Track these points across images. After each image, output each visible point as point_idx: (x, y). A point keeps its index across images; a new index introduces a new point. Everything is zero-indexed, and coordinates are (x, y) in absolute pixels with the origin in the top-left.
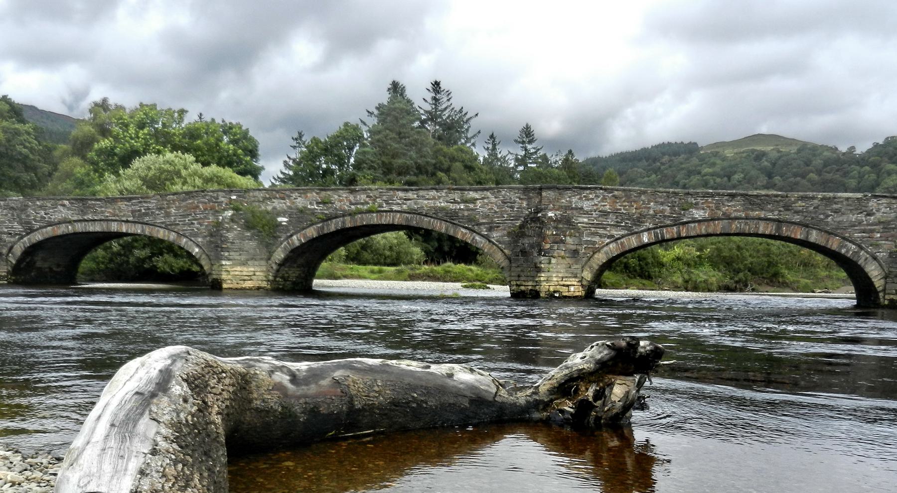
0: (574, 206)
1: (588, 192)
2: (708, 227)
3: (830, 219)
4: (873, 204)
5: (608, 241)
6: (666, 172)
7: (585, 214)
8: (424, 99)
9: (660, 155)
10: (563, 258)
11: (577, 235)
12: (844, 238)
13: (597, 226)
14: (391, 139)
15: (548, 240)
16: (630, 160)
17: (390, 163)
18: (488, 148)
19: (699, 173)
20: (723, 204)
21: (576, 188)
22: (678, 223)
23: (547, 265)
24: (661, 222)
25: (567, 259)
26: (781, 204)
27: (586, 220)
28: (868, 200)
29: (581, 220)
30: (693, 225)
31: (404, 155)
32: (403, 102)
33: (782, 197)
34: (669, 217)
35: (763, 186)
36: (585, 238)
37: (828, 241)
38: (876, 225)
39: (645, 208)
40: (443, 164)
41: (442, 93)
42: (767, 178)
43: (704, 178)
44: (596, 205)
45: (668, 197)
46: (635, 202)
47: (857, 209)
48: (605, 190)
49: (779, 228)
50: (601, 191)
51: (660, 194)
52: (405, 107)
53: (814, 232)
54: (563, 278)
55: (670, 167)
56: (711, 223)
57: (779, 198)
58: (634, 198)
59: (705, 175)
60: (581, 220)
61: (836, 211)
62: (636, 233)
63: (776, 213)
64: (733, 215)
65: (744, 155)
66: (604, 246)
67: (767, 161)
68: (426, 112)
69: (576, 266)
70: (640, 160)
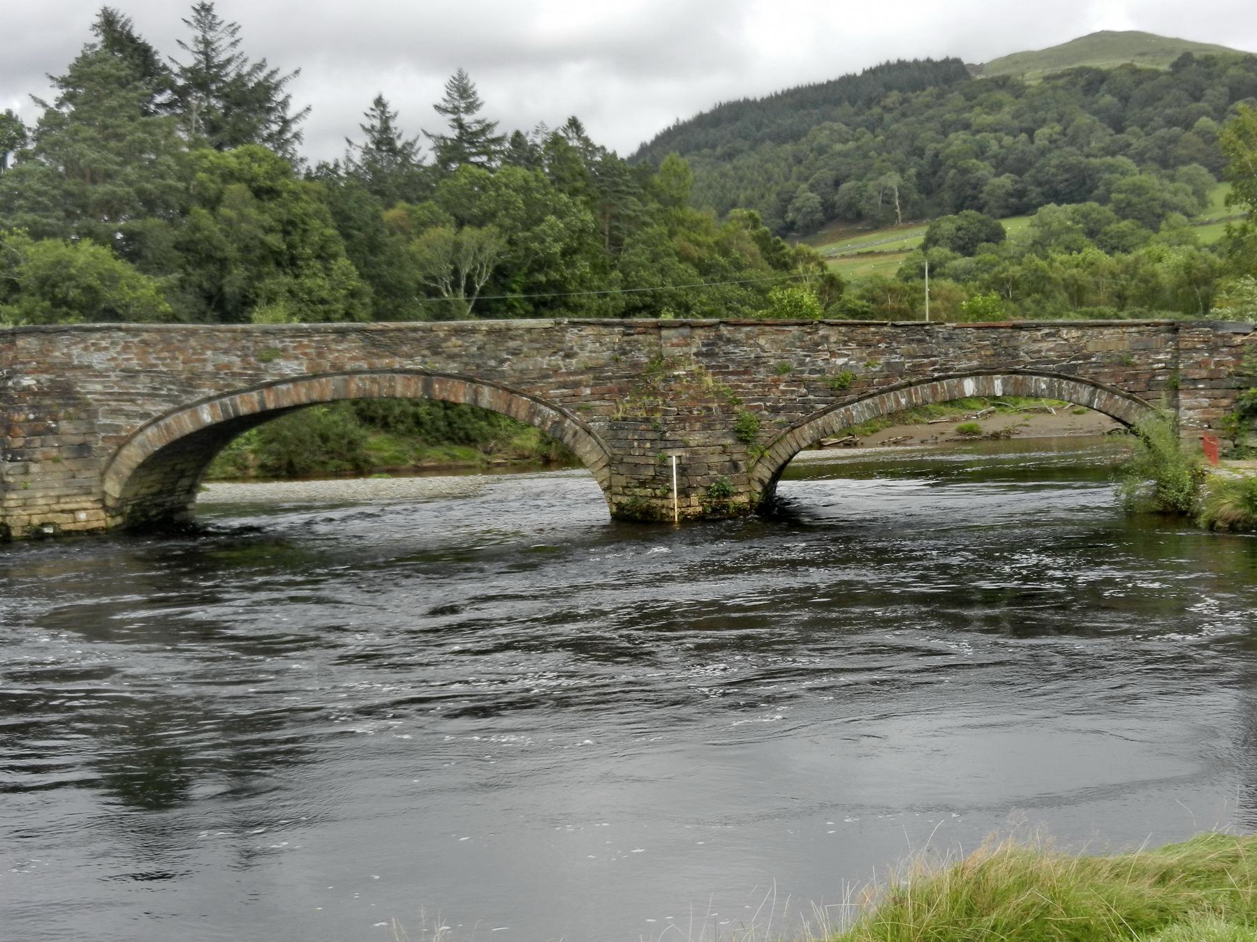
0: (76, 362)
1: (98, 335)
2: (310, 388)
3: (506, 367)
4: (571, 336)
5: (141, 423)
6: (894, 127)
7: (96, 376)
8: (180, 42)
9: (882, 89)
10: (56, 460)
11: (83, 415)
12: (534, 399)
13: (119, 397)
14: (84, 140)
15: (18, 430)
16: (815, 105)
17: (83, 194)
18: (373, 127)
19: (967, 126)
20: (329, 349)
21: (76, 329)
22: (256, 385)
23: (21, 478)
24: (228, 386)
25: (66, 463)
26: (424, 343)
27: (99, 387)
28: (564, 330)
29: (91, 387)
30: (284, 387)
31: (109, 176)
32: (112, 61)
33: (424, 331)
34: (241, 374)
35: (1102, 149)
36: (103, 421)
37: (509, 406)
38: (582, 373)
39: (198, 360)
40: (206, 189)
41: (219, 29)
42: (1111, 131)
43: (978, 137)
44: (113, 359)
45: (235, 339)
46: (178, 349)
47: (547, 347)
48: (127, 331)
49: (427, 387)
50: (121, 334)
51: (221, 335)
52: (113, 71)
53: (486, 390)
54: (59, 497)
55: (904, 115)
56: (315, 383)
57: (420, 333)
58: (178, 344)
59: (978, 131)
60: (91, 387)
61: (515, 352)
62: (189, 406)
63: (418, 359)
64: (348, 367)
65: (1061, 82)
66: (136, 434)
67: (1109, 92)
68: (184, 70)
69: (88, 474)
70: (837, 103)
